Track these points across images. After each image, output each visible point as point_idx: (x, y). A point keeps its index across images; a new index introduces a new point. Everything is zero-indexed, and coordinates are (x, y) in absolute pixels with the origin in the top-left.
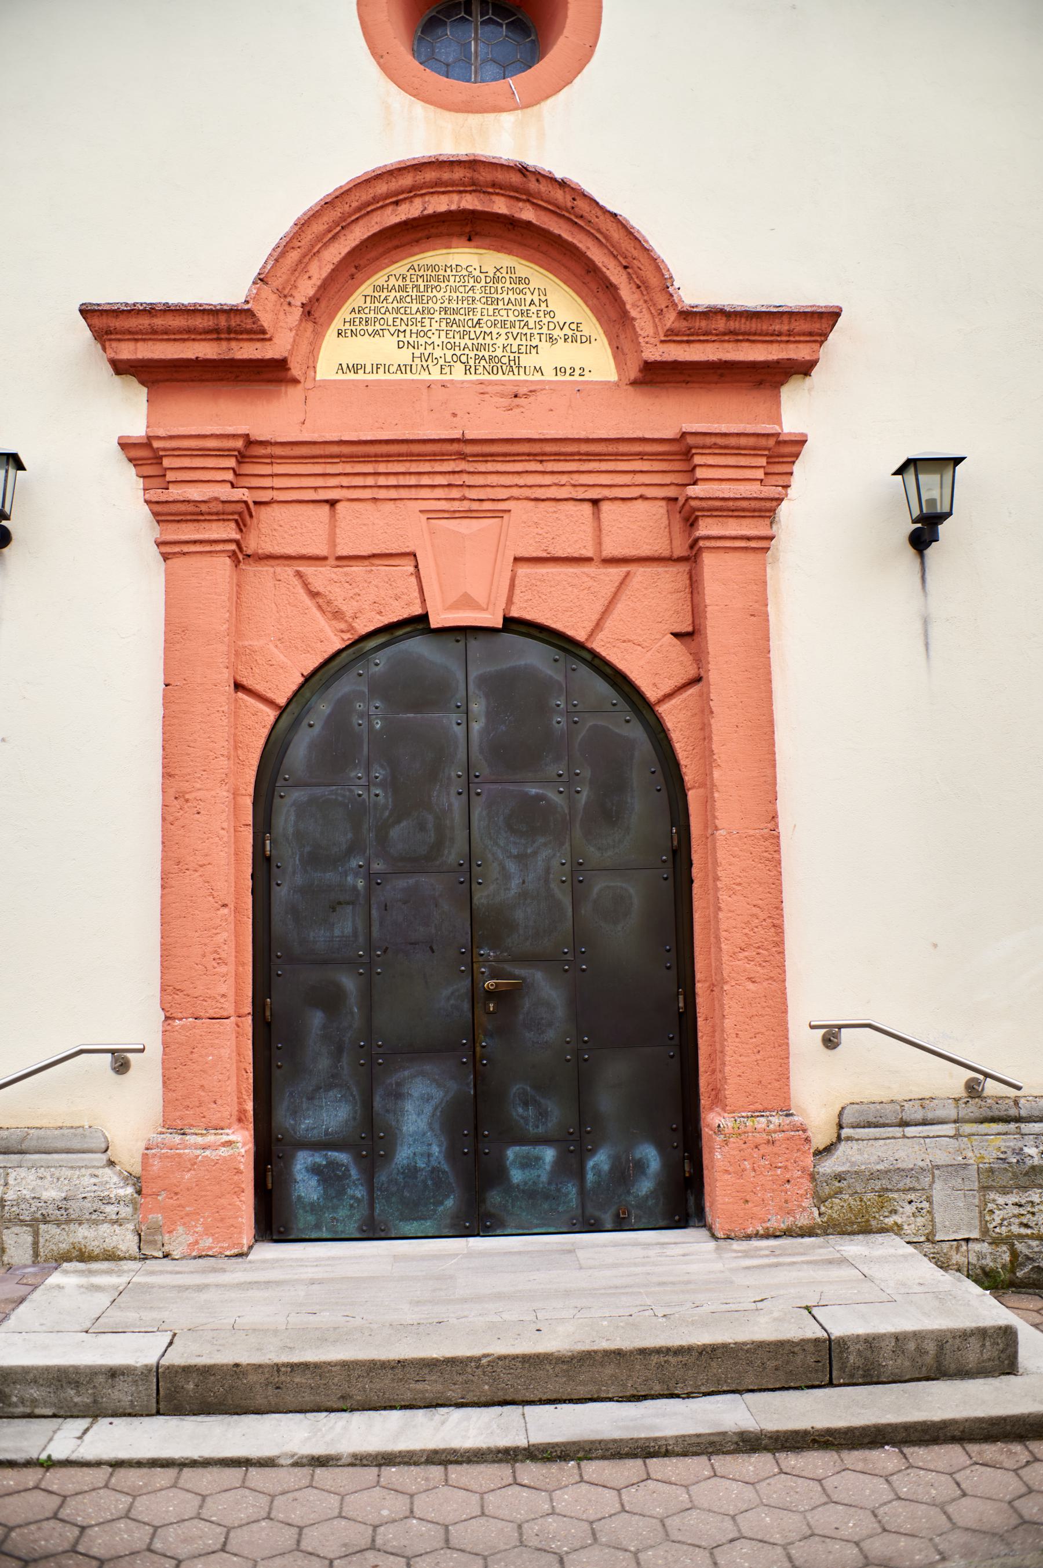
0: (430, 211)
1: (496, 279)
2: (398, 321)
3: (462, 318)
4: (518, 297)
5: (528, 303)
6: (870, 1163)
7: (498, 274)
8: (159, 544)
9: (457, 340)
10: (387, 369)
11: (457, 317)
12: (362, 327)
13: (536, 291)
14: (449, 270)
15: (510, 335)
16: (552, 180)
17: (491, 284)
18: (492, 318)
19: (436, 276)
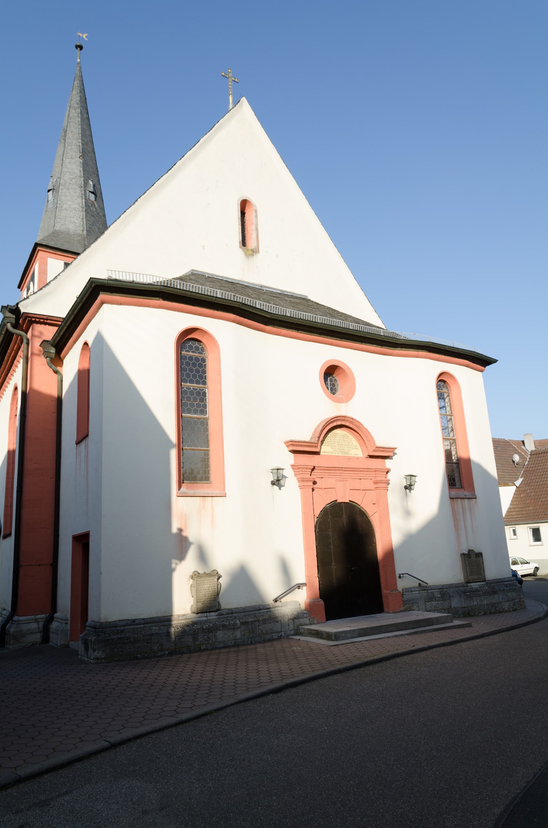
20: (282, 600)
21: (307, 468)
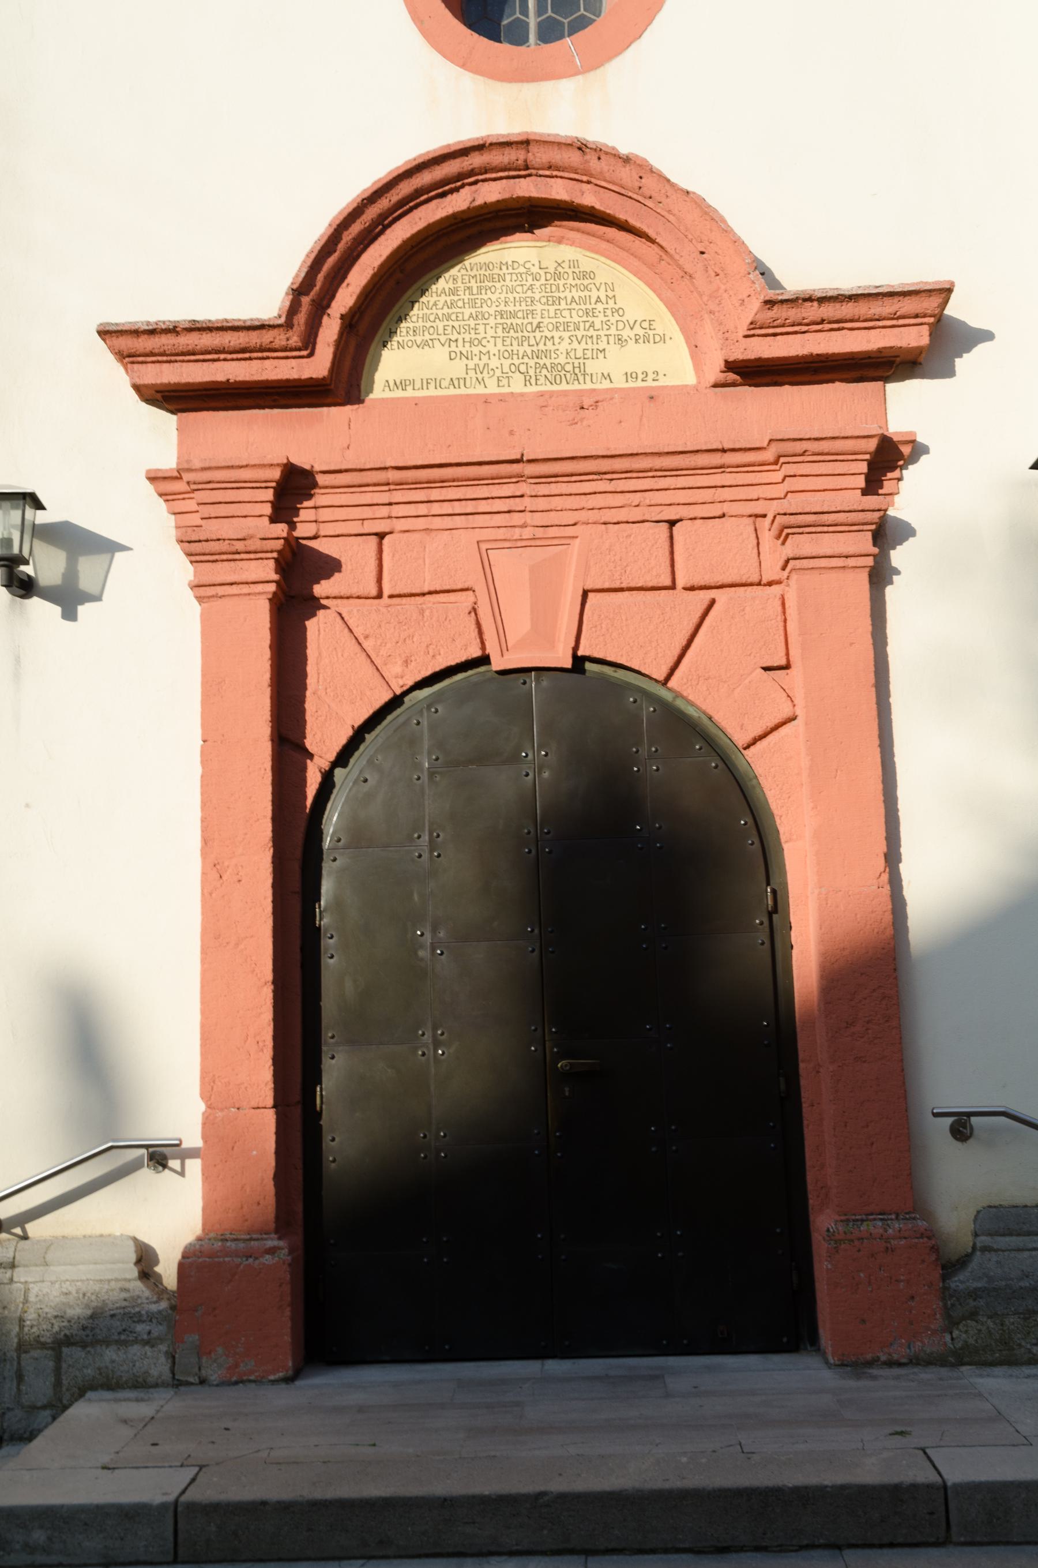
0: (479, 202)
1: (557, 276)
2: (449, 328)
3: (519, 322)
4: (582, 294)
5: (593, 300)
6: (1012, 1279)
7: (560, 269)
8: (195, 586)
9: (515, 347)
10: (438, 385)
11: (515, 321)
12: (410, 338)
13: (603, 286)
14: (504, 268)
15: (574, 339)
16: (617, 156)
17: (552, 281)
18: (554, 321)
19: (491, 277)
20: (33, 1228)
21: (239, 485)
